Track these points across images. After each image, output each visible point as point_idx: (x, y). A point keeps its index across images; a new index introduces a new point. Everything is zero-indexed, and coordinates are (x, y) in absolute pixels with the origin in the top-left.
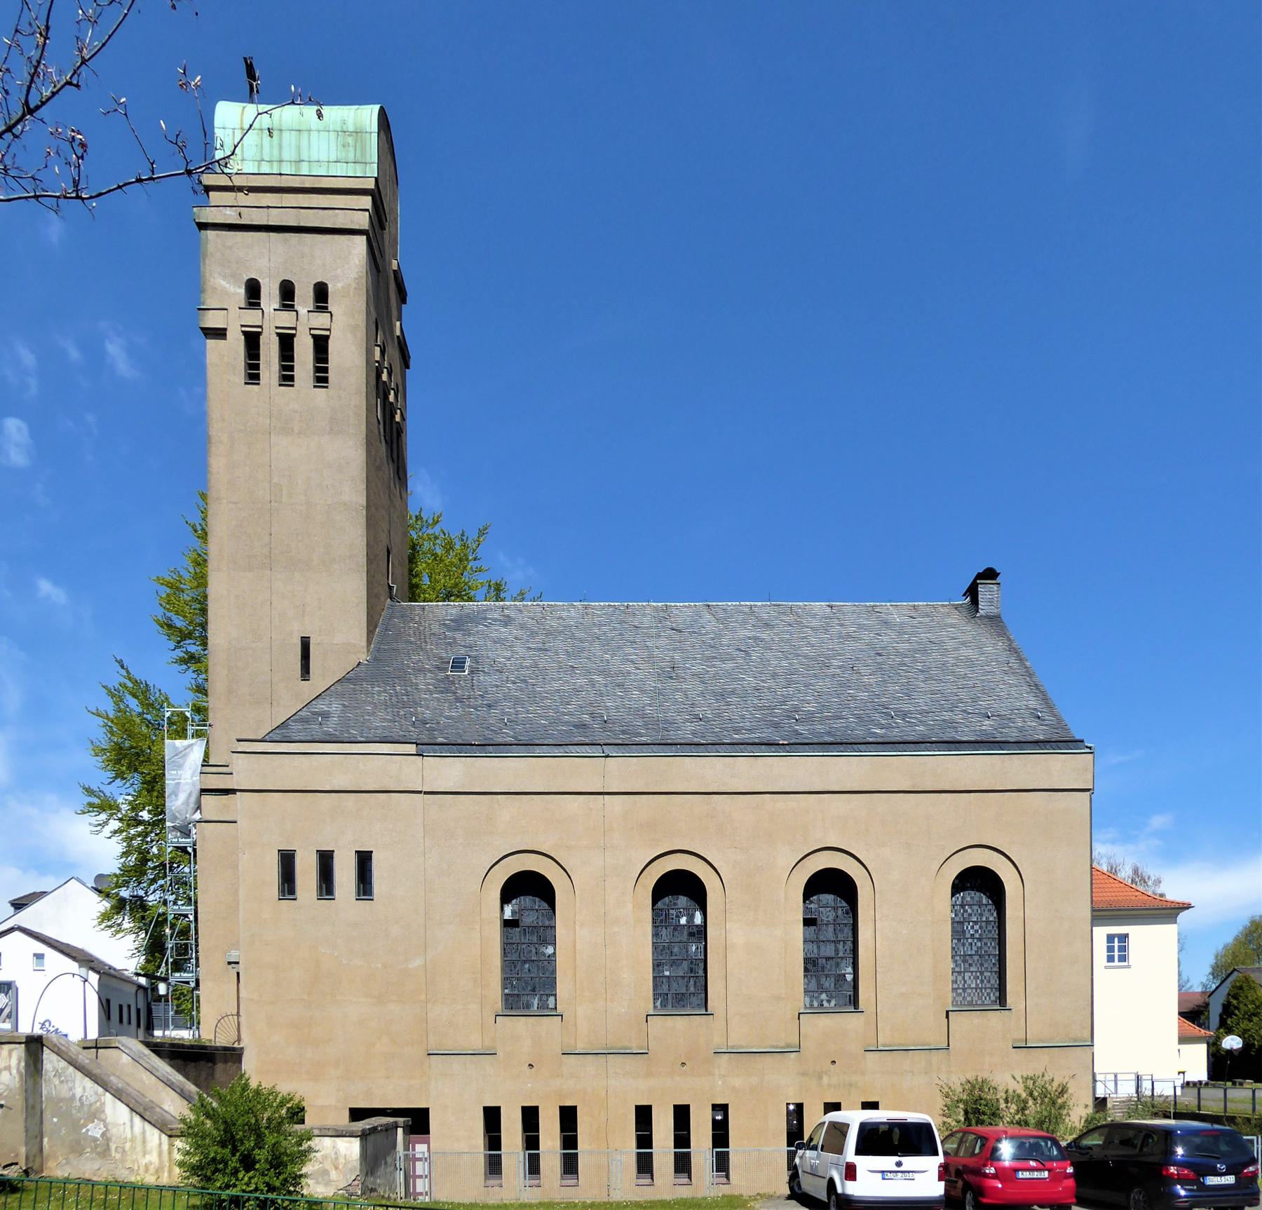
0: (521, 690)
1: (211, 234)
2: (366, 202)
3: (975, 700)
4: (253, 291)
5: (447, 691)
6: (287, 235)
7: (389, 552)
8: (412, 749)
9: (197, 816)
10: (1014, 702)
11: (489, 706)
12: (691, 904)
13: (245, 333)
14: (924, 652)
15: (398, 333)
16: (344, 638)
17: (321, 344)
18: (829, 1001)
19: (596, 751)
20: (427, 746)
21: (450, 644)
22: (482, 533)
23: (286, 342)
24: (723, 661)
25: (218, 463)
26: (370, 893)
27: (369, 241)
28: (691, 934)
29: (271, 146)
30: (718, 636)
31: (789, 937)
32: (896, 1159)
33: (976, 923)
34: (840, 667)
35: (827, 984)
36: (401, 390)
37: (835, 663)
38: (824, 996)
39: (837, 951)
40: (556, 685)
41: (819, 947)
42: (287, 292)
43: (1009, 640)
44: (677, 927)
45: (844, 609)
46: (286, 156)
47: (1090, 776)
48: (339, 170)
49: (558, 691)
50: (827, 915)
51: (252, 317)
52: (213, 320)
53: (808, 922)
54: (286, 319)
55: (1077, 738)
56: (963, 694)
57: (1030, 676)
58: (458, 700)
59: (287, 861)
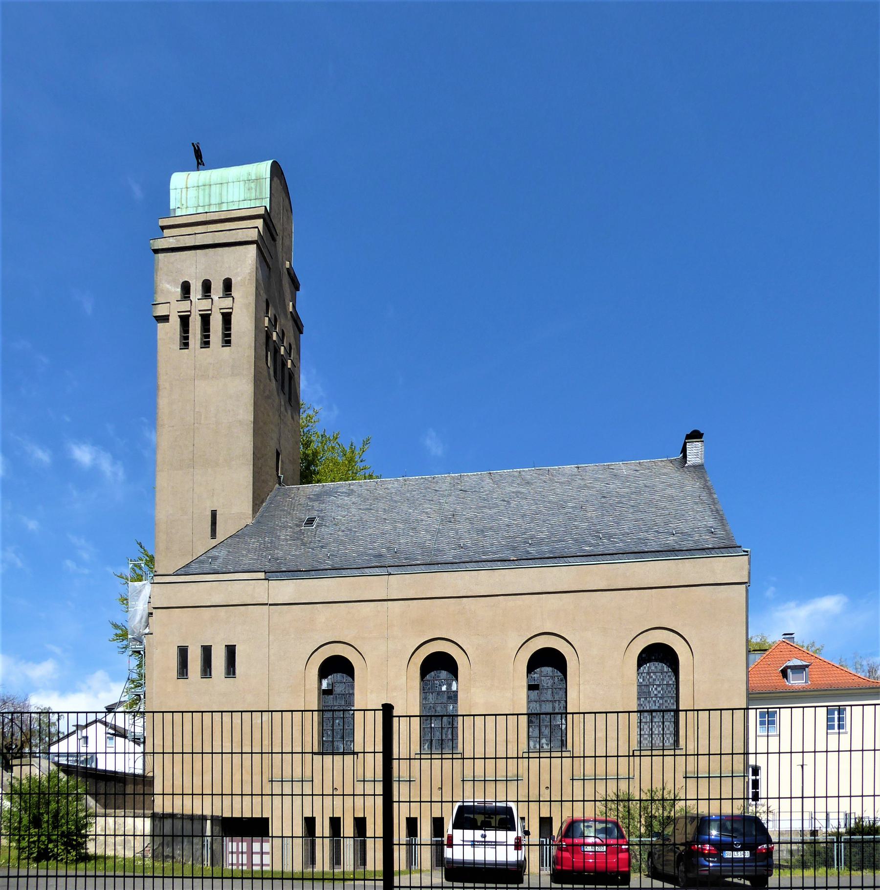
0: (347, 535)
1: (161, 256)
2: (259, 223)
3: (666, 524)
4: (186, 288)
5: (298, 539)
7: (278, 454)
8: (261, 575)
9: (147, 631)
10: (699, 521)
11: (322, 547)
12: (451, 676)
13: (180, 316)
14: (638, 493)
15: (291, 309)
16: (237, 510)
17: (227, 318)
19: (383, 571)
20: (275, 573)
21: (309, 510)
22: (365, 443)
23: (206, 319)
24: (490, 509)
25: (163, 402)
26: (234, 673)
27: (259, 248)
28: (449, 698)
29: (204, 196)
30: (492, 492)
31: (515, 695)
32: (482, 832)
33: (659, 685)
34: (573, 507)
36: (294, 349)
37: (570, 504)
39: (554, 708)
40: (370, 531)
41: (541, 706)
42: (207, 287)
43: (706, 481)
44: (440, 693)
45: (587, 469)
46: (213, 202)
47: (746, 573)
48: (247, 204)
49: (370, 535)
50: (546, 682)
51: (185, 306)
52: (161, 311)
53: (531, 687)
54: (205, 304)
55: (738, 545)
56: (659, 520)
57: (714, 503)
58: (304, 544)
59: (183, 652)
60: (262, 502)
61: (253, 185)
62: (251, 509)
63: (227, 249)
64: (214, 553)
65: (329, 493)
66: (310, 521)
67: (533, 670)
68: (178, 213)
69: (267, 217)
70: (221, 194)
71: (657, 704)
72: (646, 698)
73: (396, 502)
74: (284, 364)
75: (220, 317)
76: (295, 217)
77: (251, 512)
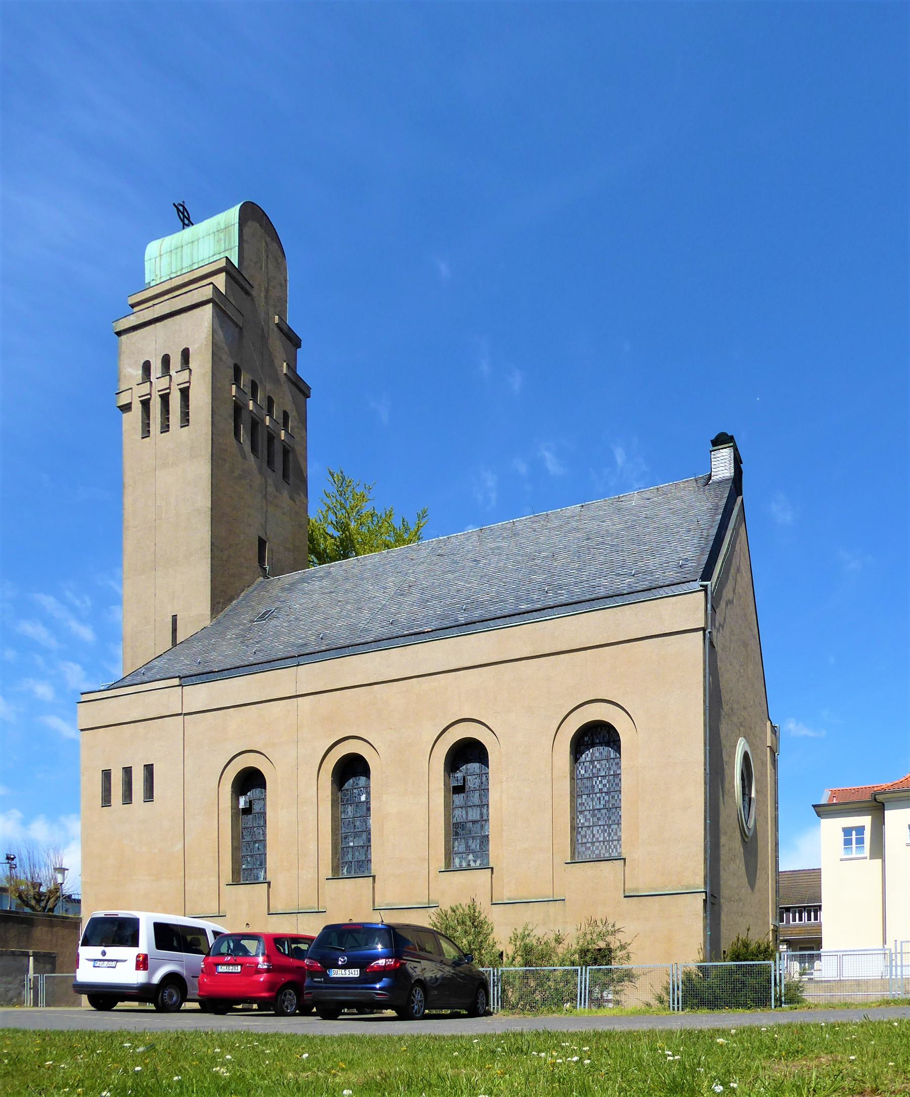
1: (124, 338)
4: (147, 367)
7: (262, 543)
8: (176, 681)
18: (475, 861)
23: (165, 399)
27: (216, 305)
32: (102, 948)
35: (473, 846)
38: (471, 857)
52: (124, 400)
54: (163, 383)
60: (231, 600)
61: (222, 235)
63: (184, 315)
64: (156, 663)
65: (303, 580)
67: (458, 769)
68: (153, 284)
70: (192, 254)
71: (603, 802)
72: (588, 795)
77: (209, 613)
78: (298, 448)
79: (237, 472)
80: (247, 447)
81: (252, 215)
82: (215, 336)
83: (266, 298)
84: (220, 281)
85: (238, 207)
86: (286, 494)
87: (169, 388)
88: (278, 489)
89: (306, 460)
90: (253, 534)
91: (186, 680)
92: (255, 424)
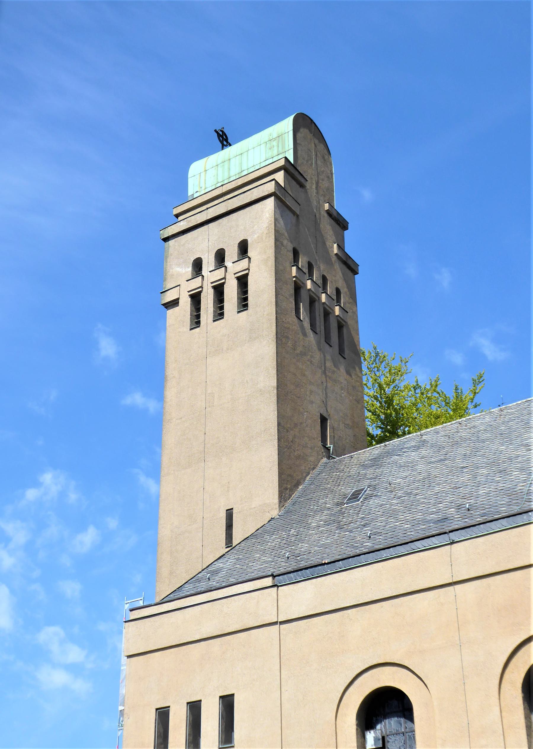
1: (171, 242)
6: (220, 221)
7: (324, 420)
8: (268, 581)
15: (336, 251)
16: (257, 496)
17: (243, 281)
23: (219, 290)
36: (347, 294)
52: (169, 297)
58: (340, 528)
60: (297, 485)
62: (277, 496)
64: (219, 564)
65: (389, 454)
66: (355, 496)
69: (289, 169)
73: (483, 441)
74: (327, 314)
75: (235, 282)
76: (334, 159)
77: (276, 501)
78: (350, 322)
79: (299, 350)
80: (307, 324)
81: (303, 124)
82: (278, 225)
83: (317, 188)
84: (280, 177)
85: (292, 117)
86: (342, 369)
87: (224, 278)
88: (335, 366)
89: (358, 334)
90: (314, 411)
91: (279, 579)
92: (313, 301)
